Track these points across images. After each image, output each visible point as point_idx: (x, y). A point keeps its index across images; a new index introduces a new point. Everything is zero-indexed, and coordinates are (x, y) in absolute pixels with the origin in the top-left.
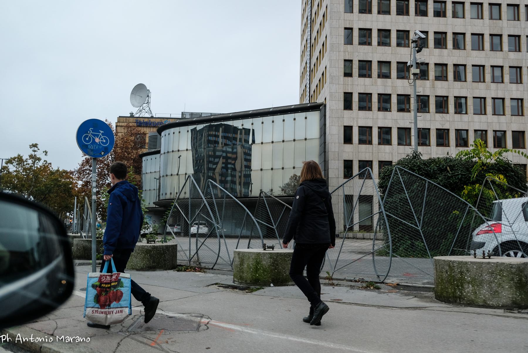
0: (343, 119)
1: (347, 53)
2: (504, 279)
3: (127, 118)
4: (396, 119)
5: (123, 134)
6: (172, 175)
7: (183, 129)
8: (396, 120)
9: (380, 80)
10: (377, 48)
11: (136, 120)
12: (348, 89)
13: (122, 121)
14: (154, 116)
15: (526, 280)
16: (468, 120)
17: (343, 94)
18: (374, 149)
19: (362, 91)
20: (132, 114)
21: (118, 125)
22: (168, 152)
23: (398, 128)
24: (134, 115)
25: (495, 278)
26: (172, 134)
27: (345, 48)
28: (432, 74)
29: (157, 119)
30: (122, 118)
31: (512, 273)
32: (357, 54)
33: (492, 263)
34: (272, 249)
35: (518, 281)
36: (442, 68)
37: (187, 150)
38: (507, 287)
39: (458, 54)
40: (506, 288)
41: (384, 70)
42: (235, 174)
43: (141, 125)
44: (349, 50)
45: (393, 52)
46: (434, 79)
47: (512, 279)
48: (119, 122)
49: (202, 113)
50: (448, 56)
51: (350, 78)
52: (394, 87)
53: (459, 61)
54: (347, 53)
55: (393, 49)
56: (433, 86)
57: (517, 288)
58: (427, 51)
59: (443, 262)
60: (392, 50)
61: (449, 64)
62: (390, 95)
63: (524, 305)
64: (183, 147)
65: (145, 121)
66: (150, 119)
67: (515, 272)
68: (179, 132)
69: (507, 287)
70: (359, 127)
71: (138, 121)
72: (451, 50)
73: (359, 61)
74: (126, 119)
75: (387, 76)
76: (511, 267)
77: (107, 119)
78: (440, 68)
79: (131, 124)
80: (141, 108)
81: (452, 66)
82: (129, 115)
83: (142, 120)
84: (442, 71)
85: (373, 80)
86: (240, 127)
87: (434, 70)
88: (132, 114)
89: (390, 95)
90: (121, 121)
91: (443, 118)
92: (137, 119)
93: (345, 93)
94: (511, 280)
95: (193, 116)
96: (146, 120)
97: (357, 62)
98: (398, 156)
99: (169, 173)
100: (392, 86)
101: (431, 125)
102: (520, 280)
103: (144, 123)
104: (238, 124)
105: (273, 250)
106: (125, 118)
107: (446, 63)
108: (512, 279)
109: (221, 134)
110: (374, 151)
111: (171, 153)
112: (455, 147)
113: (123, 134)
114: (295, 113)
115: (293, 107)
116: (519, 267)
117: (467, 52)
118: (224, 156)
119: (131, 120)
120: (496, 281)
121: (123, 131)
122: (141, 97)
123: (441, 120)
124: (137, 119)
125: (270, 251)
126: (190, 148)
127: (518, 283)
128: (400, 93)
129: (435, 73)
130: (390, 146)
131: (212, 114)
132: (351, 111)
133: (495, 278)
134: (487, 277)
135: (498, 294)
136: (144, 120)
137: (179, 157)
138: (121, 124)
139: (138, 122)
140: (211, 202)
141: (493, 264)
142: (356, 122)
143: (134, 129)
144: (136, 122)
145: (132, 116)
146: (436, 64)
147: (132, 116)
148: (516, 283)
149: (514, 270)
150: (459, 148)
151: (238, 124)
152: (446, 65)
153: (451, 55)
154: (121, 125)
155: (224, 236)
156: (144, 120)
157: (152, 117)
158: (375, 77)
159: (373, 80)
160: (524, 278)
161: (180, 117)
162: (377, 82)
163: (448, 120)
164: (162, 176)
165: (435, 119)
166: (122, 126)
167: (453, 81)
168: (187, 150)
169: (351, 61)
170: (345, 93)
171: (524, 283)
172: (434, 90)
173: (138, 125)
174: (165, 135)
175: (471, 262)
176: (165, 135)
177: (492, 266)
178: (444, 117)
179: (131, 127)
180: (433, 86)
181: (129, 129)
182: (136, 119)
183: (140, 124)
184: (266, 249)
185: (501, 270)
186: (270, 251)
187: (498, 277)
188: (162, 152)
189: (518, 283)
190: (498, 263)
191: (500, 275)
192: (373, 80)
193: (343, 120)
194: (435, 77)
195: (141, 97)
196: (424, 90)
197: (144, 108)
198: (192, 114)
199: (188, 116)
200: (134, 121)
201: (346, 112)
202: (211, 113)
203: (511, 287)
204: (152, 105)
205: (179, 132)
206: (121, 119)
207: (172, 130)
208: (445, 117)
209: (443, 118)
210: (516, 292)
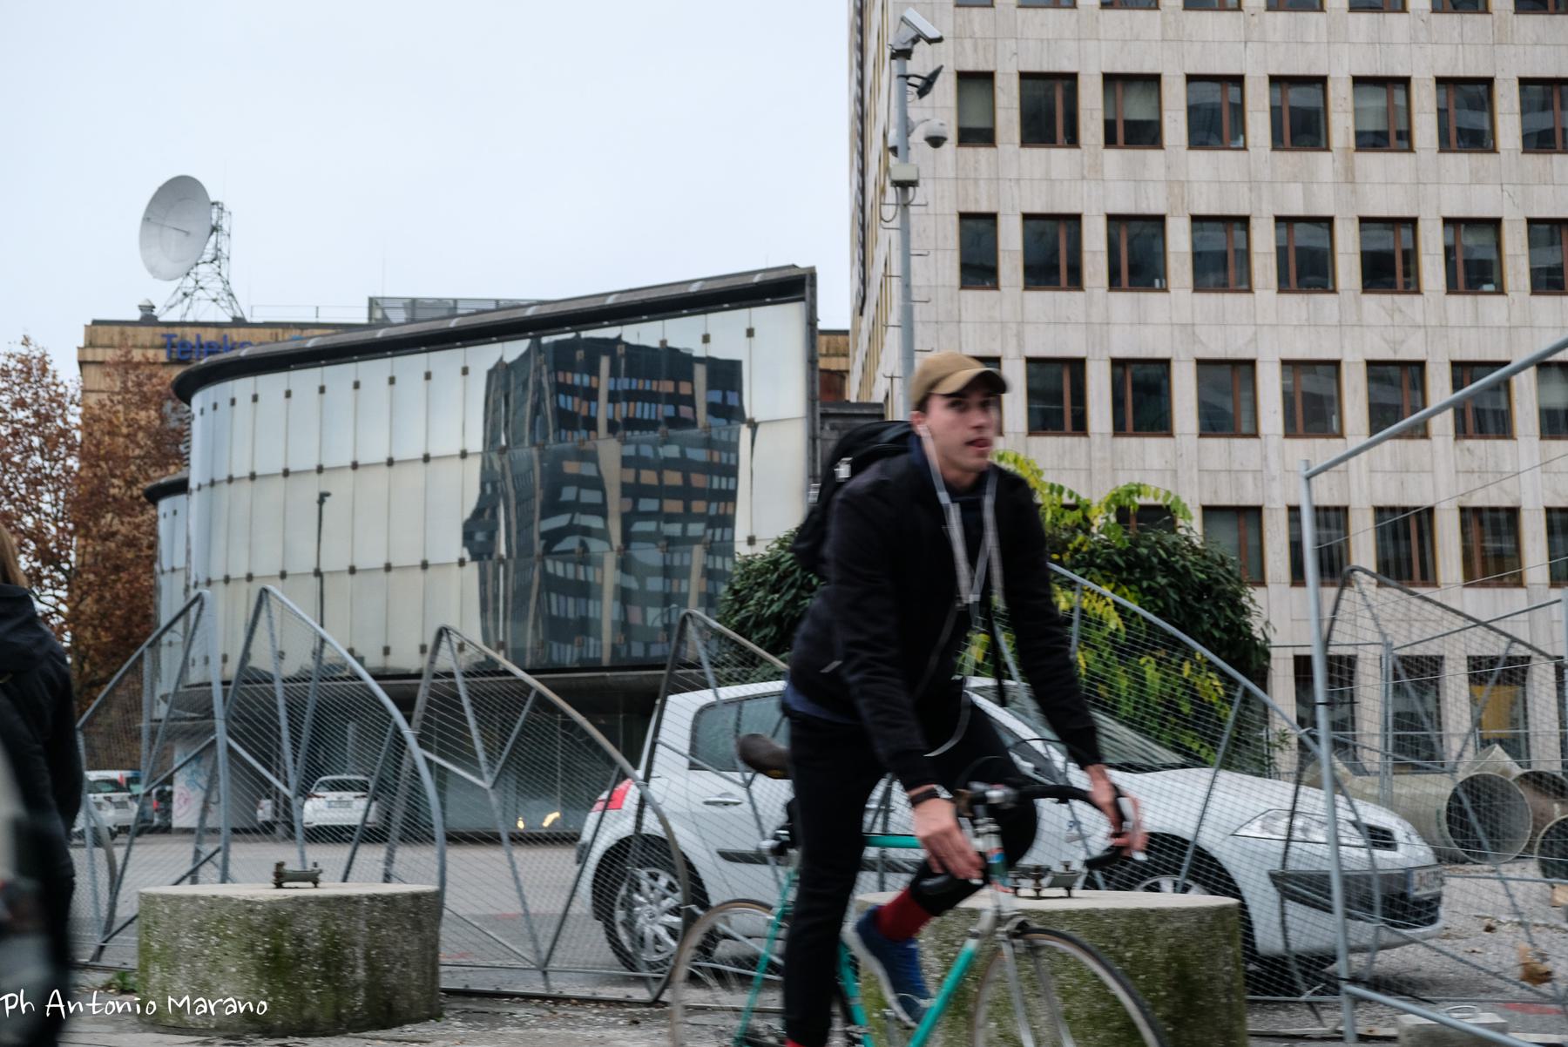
0: (959, 328)
1: (968, 44)
2: (228, 945)
3: (129, 330)
4: (1190, 322)
5: (105, 396)
6: (227, 580)
7: (446, 361)
8: (1189, 328)
9: (1114, 156)
10: (1097, 18)
11: (163, 335)
12: (977, 201)
13: (106, 341)
14: (249, 319)
15: (295, 951)
16: (1509, 319)
17: (956, 219)
18: (1097, 454)
19: (1038, 208)
20: (148, 309)
21: (89, 358)
22: (213, 483)
23: (1201, 363)
24: (156, 312)
25: (206, 944)
26: (244, 400)
27: (959, 20)
28: (1341, 124)
29: (255, 331)
30: (106, 328)
31: (251, 928)
32: (1011, 44)
33: (204, 898)
34: (310, 884)
35: (268, 951)
36: (1390, 98)
37: (464, 455)
38: (234, 970)
39: (1456, 34)
40: (231, 973)
41: (1136, 108)
42: (686, 562)
43: (186, 356)
44: (977, 27)
45: (1171, 34)
46: (1352, 144)
47: (251, 947)
48: (91, 344)
49: (455, 301)
50: (1414, 41)
51: (983, 152)
52: (1177, 186)
53: (1460, 63)
54: (968, 44)
55: (1171, 18)
56: (1350, 176)
57: (261, 972)
58: (1317, 25)
59: (409, 904)
60: (1164, 24)
61: (1415, 76)
62: (1160, 220)
63: (282, 1025)
64: (446, 442)
65: (203, 341)
66: (226, 331)
67: (262, 926)
68: (255, 398)
69: (234, 970)
70: (1030, 360)
71: (175, 340)
72: (1426, 15)
73: (1024, 76)
74: (122, 333)
75: (1144, 135)
76: (251, 911)
77: (27, 334)
78: (1376, 100)
79: (137, 355)
80: (190, 282)
81: (1433, 84)
82: (136, 315)
83: (190, 335)
84: (1389, 111)
85: (1082, 155)
86: (699, 351)
87: (1349, 105)
88: (148, 309)
89: (1160, 220)
90: (99, 342)
91: (1397, 317)
92: (170, 331)
93: (964, 216)
94: (245, 950)
95: (420, 314)
96: (210, 336)
97: (1015, 83)
98: (1200, 483)
99: (217, 575)
100: (1169, 183)
101: (1342, 347)
102: (277, 950)
103: (201, 346)
104: (681, 333)
105: (1069, 896)
106: (116, 329)
107: (1400, 72)
108: (251, 947)
109: (604, 383)
110: (1096, 465)
111: (245, 488)
112: (1451, 438)
113: (105, 396)
114: (705, 313)
115: (694, 288)
116: (277, 911)
117: (1497, 24)
118: (630, 484)
119: (146, 334)
120: (207, 952)
121: (104, 384)
122: (188, 233)
123: (1389, 321)
124: (170, 331)
125: (305, 890)
126: (476, 443)
127: (267, 958)
128: (1202, 210)
129: (1356, 122)
130: (1166, 441)
131: (499, 306)
132: (993, 293)
133: (206, 944)
134: (187, 941)
135: (210, 990)
136: (198, 337)
137: (321, 501)
138: (100, 355)
139: (173, 346)
140: (446, 692)
141: (202, 902)
142: (1013, 342)
143: (150, 377)
144: (169, 345)
145: (149, 318)
146: (1358, 81)
147: (149, 318)
148: (260, 958)
149: (256, 920)
150: (1469, 443)
151: (681, 333)
152: (1405, 82)
153: (1422, 36)
154: (99, 359)
155: (505, 837)
156: (198, 337)
157: (238, 322)
158: (1093, 142)
159: (1082, 155)
160: (291, 944)
161: (361, 317)
162: (1102, 165)
163: (1419, 319)
164: (192, 583)
165: (1359, 320)
166: (101, 363)
167: (1435, 152)
168: (464, 455)
169: (987, 77)
170: (964, 216)
171: (290, 958)
172: (1354, 192)
173: (174, 356)
174: (215, 407)
175: (162, 896)
176: (215, 407)
177: (201, 906)
178: (1401, 311)
179: (137, 365)
180: (1350, 176)
181: (132, 377)
182: (164, 330)
183: (183, 353)
184: (1045, 893)
185: (221, 920)
186: (305, 890)
187: (214, 939)
188: (193, 485)
189: (267, 958)
190: (214, 897)
191: (217, 935)
192: (1085, 158)
193: (960, 334)
194: (1359, 135)
195: (188, 233)
196: (1308, 195)
197: (201, 284)
198: (413, 304)
199: (398, 316)
200: (159, 341)
201: (974, 297)
202: (497, 301)
203: (243, 971)
204: (238, 270)
205: (255, 398)
206: (103, 335)
207: (241, 387)
208: (1404, 308)
209: (1397, 317)
210: (259, 984)
